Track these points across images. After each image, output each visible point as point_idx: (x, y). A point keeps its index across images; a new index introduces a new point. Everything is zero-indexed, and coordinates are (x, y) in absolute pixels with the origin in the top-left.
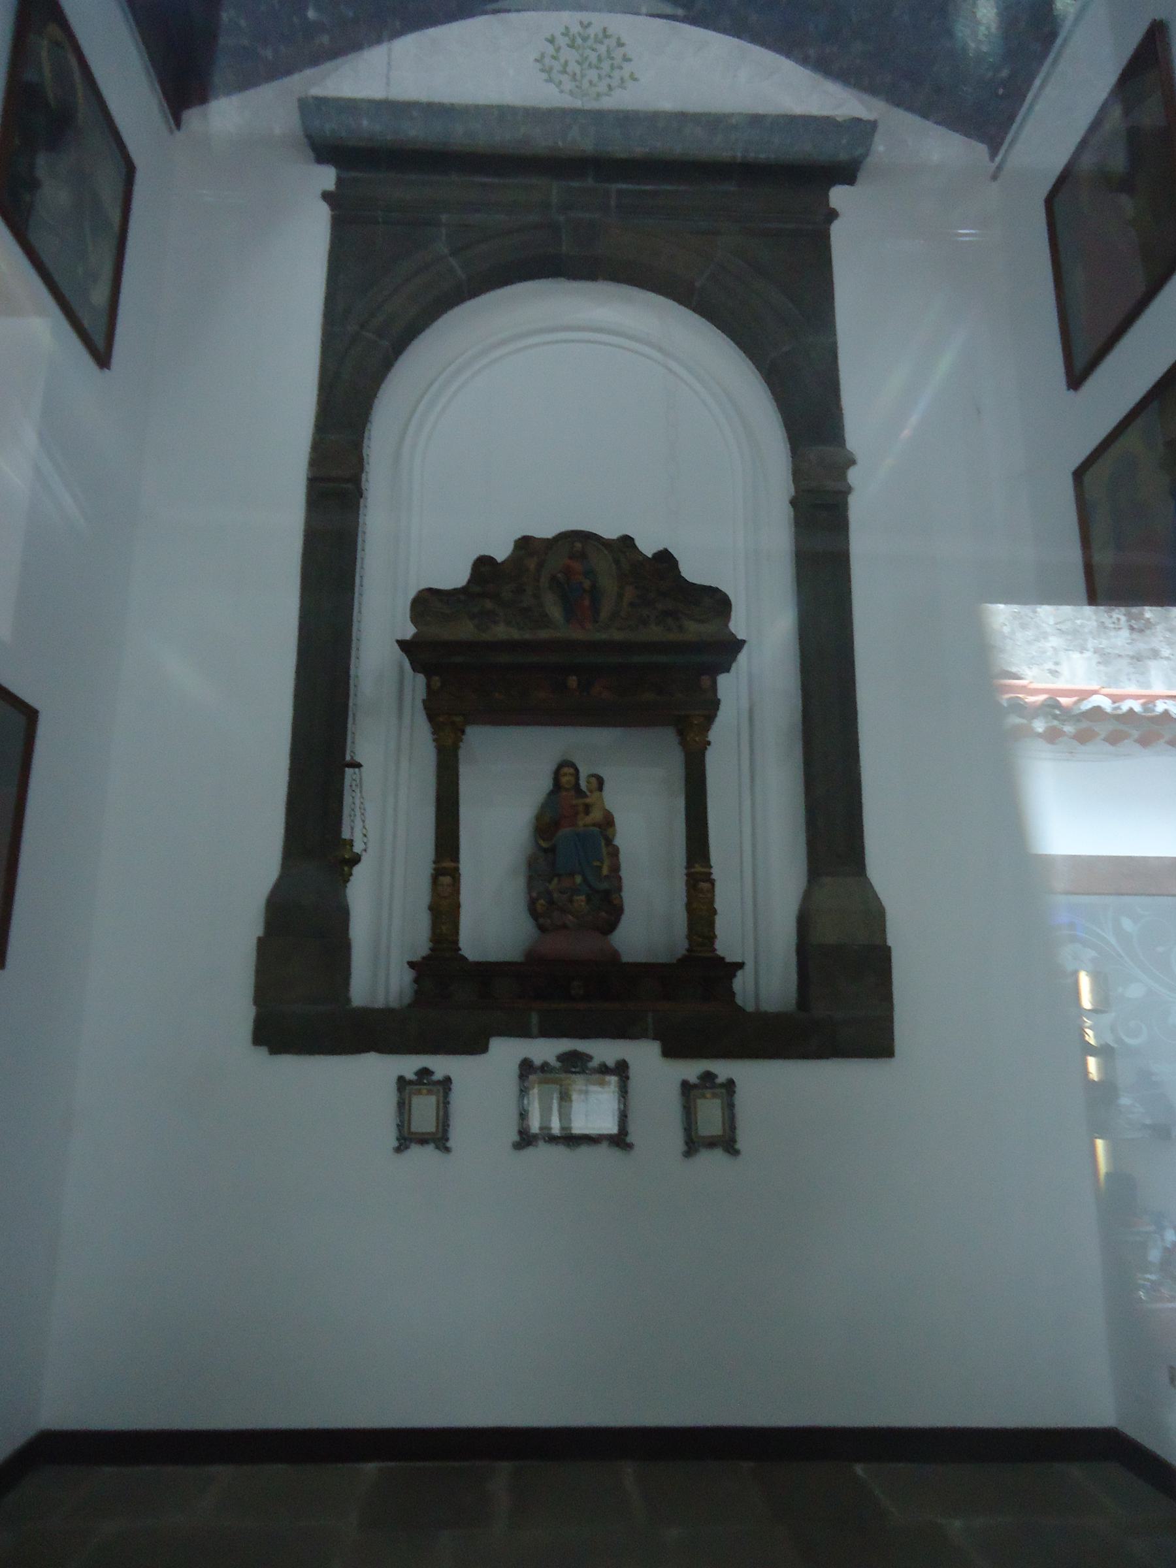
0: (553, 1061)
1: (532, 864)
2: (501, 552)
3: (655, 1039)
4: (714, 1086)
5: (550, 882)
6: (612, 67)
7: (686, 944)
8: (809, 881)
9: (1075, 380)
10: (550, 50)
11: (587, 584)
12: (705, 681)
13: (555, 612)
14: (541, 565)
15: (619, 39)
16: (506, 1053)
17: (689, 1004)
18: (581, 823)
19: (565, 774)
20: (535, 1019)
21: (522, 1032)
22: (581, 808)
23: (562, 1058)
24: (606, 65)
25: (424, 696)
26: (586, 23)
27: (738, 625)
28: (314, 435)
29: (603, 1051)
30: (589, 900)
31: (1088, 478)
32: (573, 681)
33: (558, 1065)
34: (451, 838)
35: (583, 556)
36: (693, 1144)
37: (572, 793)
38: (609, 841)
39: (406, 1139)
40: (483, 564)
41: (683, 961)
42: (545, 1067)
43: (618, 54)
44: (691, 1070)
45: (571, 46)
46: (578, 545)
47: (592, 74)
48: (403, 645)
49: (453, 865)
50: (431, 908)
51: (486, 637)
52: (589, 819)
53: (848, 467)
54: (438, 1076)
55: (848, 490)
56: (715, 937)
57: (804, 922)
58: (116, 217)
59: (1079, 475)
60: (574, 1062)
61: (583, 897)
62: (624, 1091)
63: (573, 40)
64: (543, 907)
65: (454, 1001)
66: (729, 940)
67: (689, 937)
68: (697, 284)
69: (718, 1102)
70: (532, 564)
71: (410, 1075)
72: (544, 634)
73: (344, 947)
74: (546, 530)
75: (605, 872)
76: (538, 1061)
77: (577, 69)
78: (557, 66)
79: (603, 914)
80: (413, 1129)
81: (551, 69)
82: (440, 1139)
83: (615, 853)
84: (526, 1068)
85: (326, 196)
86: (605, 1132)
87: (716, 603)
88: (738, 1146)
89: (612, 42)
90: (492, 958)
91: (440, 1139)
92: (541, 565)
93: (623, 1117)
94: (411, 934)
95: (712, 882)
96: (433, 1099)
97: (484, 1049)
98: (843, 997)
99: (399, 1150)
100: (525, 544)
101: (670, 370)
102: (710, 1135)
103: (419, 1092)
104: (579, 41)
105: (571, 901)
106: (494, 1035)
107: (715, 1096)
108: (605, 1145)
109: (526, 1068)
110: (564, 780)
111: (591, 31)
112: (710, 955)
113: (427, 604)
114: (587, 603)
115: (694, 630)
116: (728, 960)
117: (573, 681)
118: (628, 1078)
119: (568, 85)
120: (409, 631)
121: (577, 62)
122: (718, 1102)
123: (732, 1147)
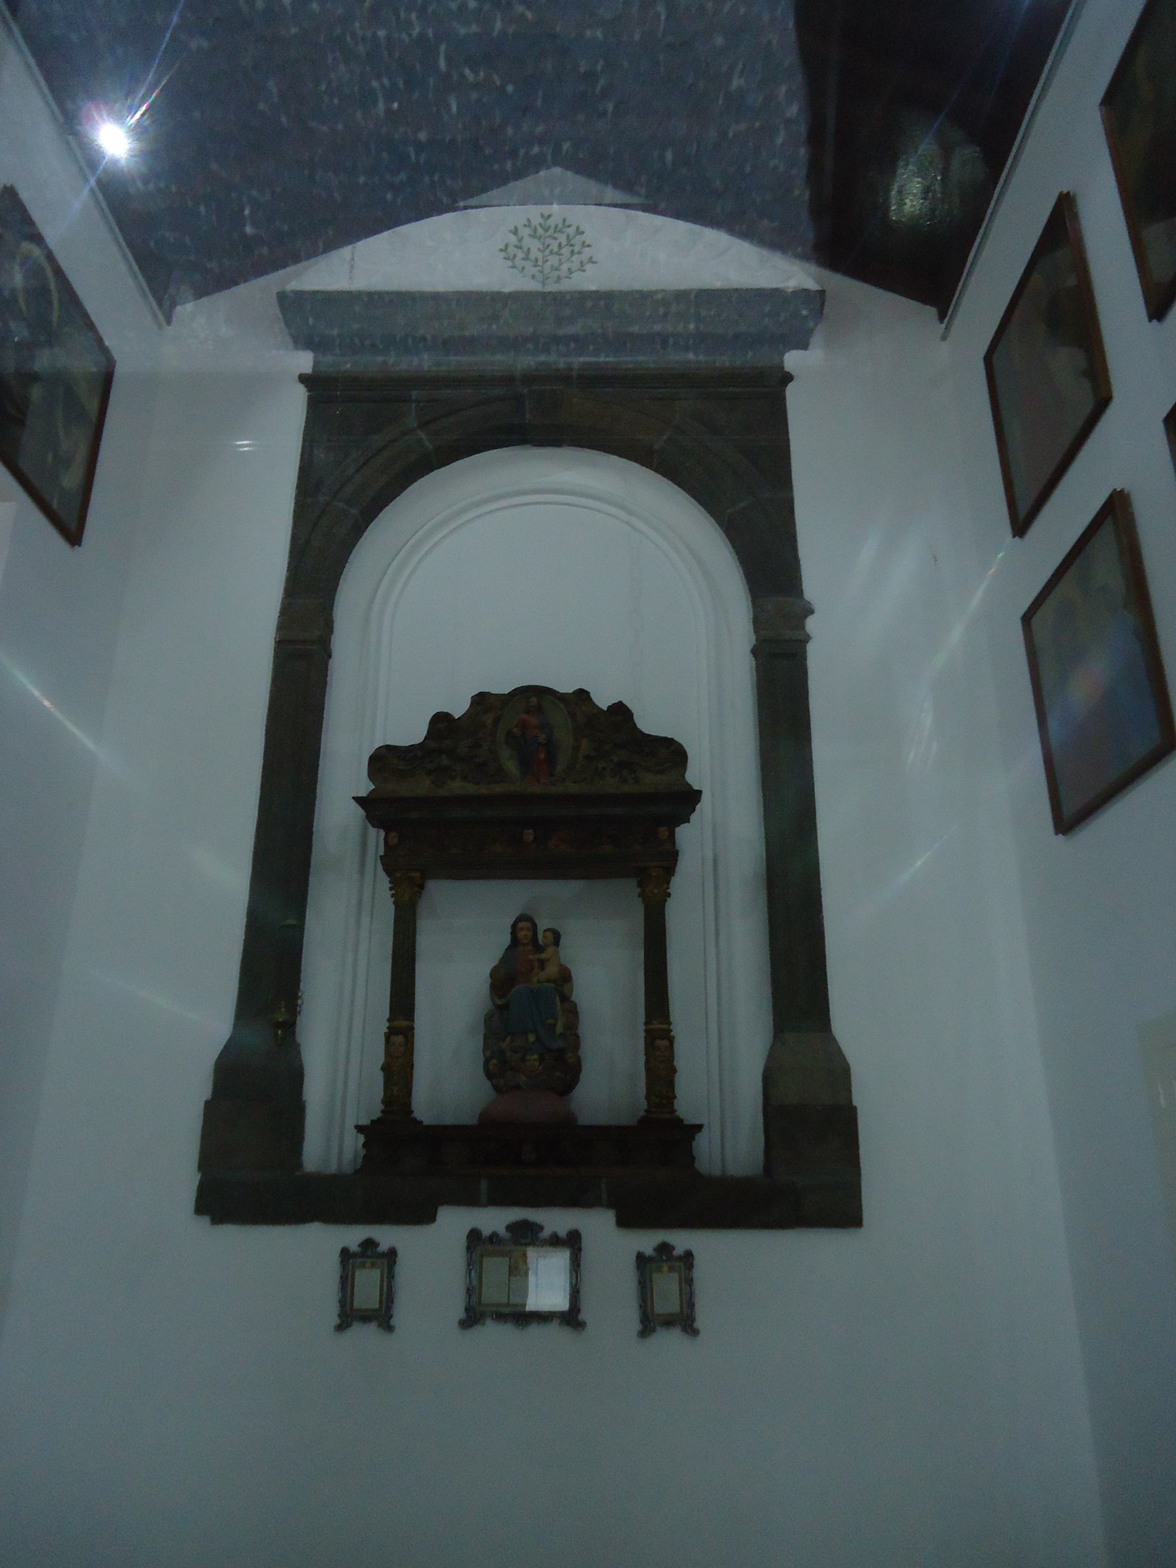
0: (502, 1230)
1: (488, 1019)
2: (459, 708)
3: (609, 1206)
4: (671, 1258)
5: (504, 1040)
6: (572, 253)
7: (644, 1104)
8: (775, 1036)
9: (1020, 527)
10: (513, 239)
11: (542, 738)
12: (663, 831)
13: (511, 766)
14: (496, 722)
15: (578, 228)
16: (454, 1224)
17: (649, 1171)
18: (535, 979)
19: (522, 929)
20: (484, 1185)
21: (470, 1200)
22: (536, 964)
23: (513, 1228)
24: (566, 251)
25: (381, 852)
26: (546, 215)
27: (695, 775)
28: (284, 599)
29: (556, 1220)
30: (542, 1059)
31: (1035, 620)
32: (529, 835)
33: (507, 1235)
34: (401, 997)
35: (539, 710)
36: (649, 1323)
37: (530, 948)
38: (565, 999)
39: (349, 1316)
40: (441, 722)
41: (643, 1121)
42: (494, 1238)
43: (577, 240)
44: (647, 1241)
45: (533, 235)
46: (534, 700)
47: (553, 260)
48: (358, 800)
49: (405, 1023)
50: (383, 1068)
51: (443, 792)
52: (543, 975)
53: (806, 617)
54: (384, 1247)
55: (807, 638)
56: (675, 1097)
57: (769, 1079)
58: (93, 406)
59: (1027, 619)
60: (525, 1233)
61: (535, 1057)
62: (576, 1265)
63: (535, 230)
64: (498, 1066)
65: (408, 1167)
66: (692, 1096)
67: (648, 1097)
68: (656, 447)
69: (675, 1276)
70: (488, 719)
71: (354, 1247)
72: (498, 789)
73: (298, 1110)
74: (503, 687)
75: (559, 1029)
76: (486, 1232)
77: (540, 256)
78: (520, 255)
79: (558, 1074)
80: (356, 1305)
81: (515, 256)
82: (382, 1316)
83: (573, 1012)
84: (474, 1237)
85: (303, 379)
86: (558, 1309)
87: (672, 754)
88: (697, 1325)
89: (571, 231)
90: (449, 1120)
91: (382, 1316)
92: (496, 722)
93: (575, 1294)
94: (365, 1098)
95: (671, 1040)
96: (376, 1273)
97: (431, 1219)
98: (810, 1164)
99: (341, 1327)
100: (481, 700)
101: (634, 529)
102: (667, 1313)
103: (363, 1266)
104: (540, 231)
105: (523, 1059)
106: (442, 1204)
107: (671, 1269)
108: (556, 1323)
109: (474, 1237)
110: (521, 935)
111: (551, 222)
112: (667, 1116)
113: (384, 761)
114: (542, 756)
115: (650, 781)
116: (686, 1122)
117: (529, 835)
118: (580, 1250)
119: (531, 270)
120: (365, 787)
121: (539, 250)
122: (675, 1276)
123: (691, 1326)
